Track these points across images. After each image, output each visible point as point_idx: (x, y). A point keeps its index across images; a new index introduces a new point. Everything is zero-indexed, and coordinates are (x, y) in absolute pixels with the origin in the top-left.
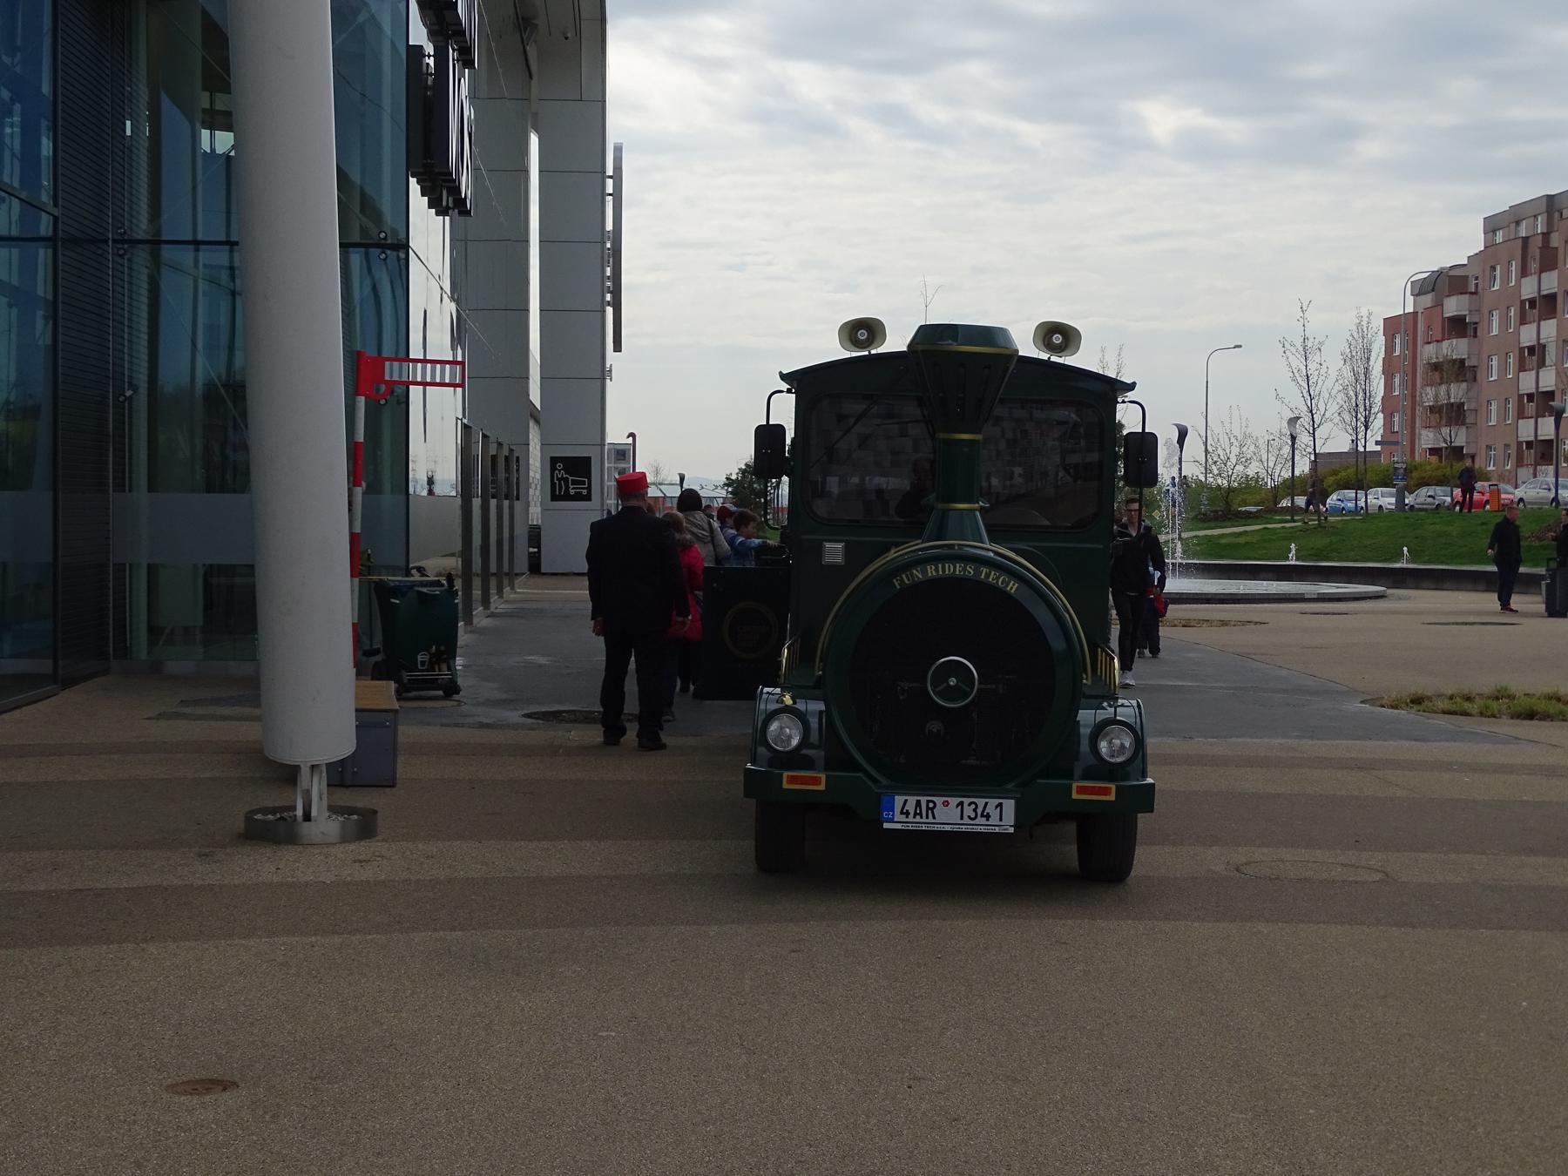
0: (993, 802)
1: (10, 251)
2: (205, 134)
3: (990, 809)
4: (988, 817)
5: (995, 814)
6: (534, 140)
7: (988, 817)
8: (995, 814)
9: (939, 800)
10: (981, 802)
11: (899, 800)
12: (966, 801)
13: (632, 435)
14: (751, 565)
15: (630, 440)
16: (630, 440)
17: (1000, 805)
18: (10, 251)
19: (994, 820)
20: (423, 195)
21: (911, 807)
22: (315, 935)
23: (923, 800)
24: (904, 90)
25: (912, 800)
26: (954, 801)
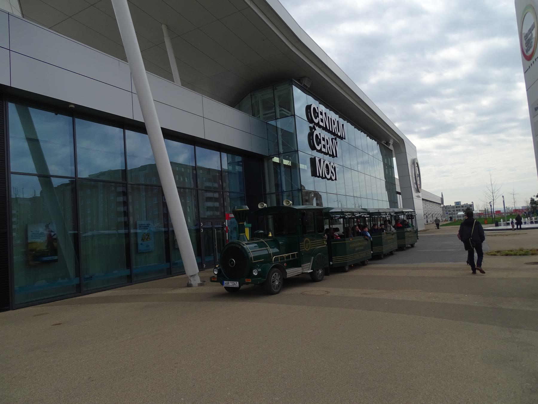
0: (236, 282)
1: (213, 194)
2: (225, 166)
3: (236, 283)
4: (235, 284)
5: (236, 284)
6: (394, 159)
7: (235, 284)
8: (236, 284)
9: (229, 282)
10: (234, 282)
11: (225, 282)
12: (233, 282)
13: (472, 202)
14: (498, 214)
15: (472, 203)
16: (472, 203)
17: (237, 283)
18: (213, 194)
19: (236, 285)
20: (89, 175)
21: (226, 283)
22: (140, 295)
23: (228, 282)
24: (502, 136)
25: (226, 282)
26: (231, 282)
